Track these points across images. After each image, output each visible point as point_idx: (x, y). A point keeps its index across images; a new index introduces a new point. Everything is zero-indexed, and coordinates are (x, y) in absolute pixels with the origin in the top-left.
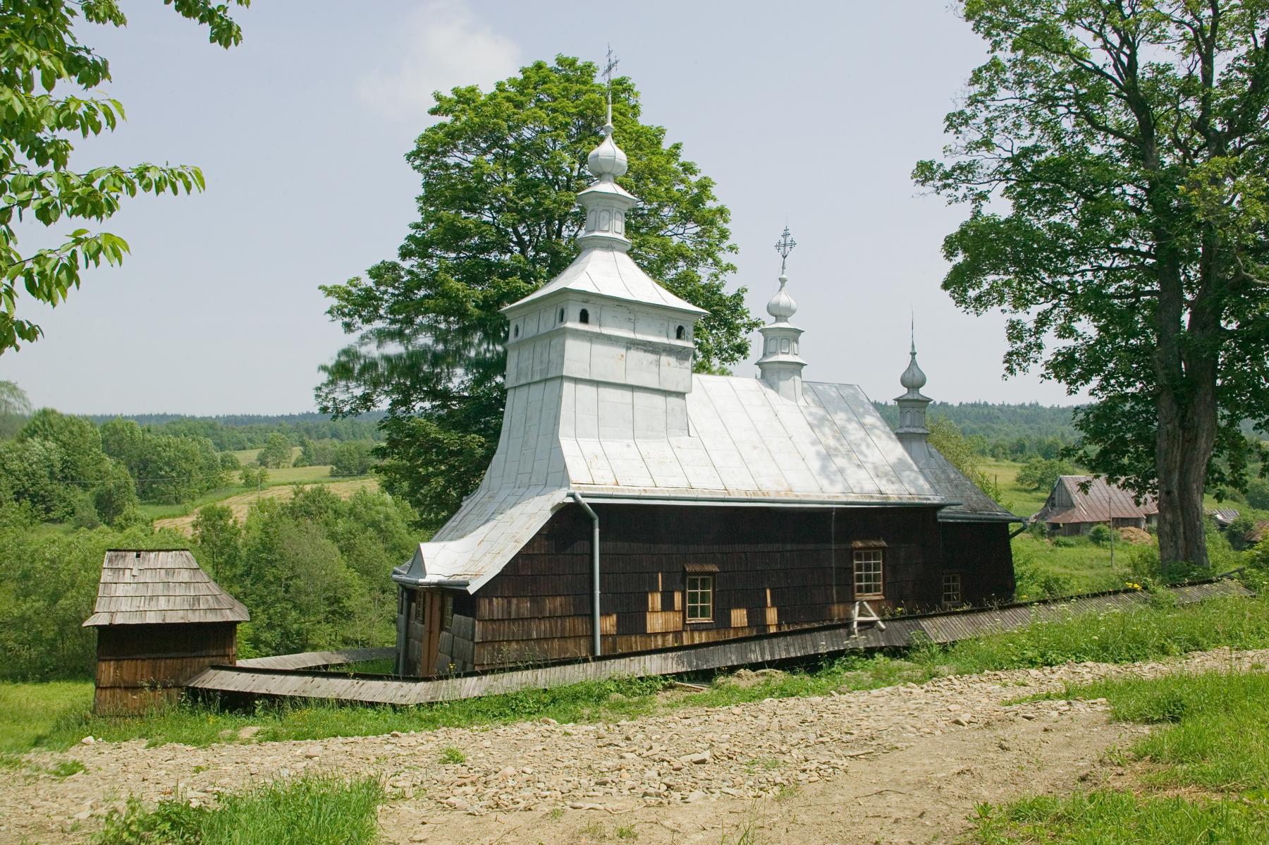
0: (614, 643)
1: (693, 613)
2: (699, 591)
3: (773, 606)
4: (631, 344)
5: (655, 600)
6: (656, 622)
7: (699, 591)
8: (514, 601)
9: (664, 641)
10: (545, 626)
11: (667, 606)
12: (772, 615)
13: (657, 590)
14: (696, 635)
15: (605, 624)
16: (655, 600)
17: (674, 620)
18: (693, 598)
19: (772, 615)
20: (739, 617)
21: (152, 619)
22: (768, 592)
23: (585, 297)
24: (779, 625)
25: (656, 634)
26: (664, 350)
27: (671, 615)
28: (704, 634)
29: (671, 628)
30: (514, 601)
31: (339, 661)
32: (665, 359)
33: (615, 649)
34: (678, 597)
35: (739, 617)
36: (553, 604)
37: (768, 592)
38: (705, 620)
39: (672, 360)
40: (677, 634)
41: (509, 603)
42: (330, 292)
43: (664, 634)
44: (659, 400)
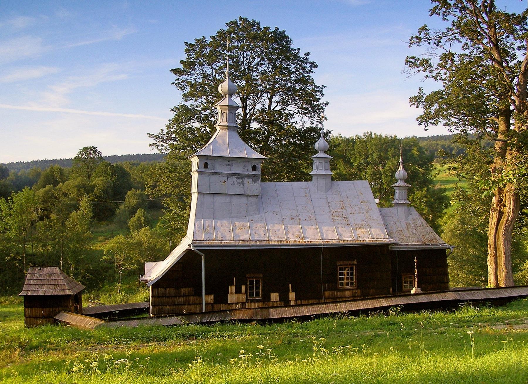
0: (213, 307)
1: (252, 294)
2: (255, 285)
3: (292, 291)
4: (229, 175)
5: (232, 289)
6: (232, 298)
7: (255, 285)
8: (168, 289)
9: (251, 305)
10: (182, 299)
11: (238, 291)
12: (292, 296)
13: (233, 285)
14: (253, 304)
15: (207, 299)
16: (232, 289)
17: (242, 297)
18: (251, 288)
19: (292, 296)
20: (274, 296)
21: (41, 293)
22: (290, 285)
23: (206, 157)
24: (296, 300)
25: (232, 304)
26: (246, 177)
27: (240, 295)
28: (256, 304)
29: (240, 301)
30: (168, 289)
31: (18, 328)
32: (246, 180)
33: (213, 309)
34: (243, 288)
35: (274, 296)
36: (185, 290)
37: (290, 285)
38: (257, 298)
39: (250, 181)
40: (243, 304)
41: (166, 289)
42: (150, 135)
43: (237, 304)
44: (244, 200)
